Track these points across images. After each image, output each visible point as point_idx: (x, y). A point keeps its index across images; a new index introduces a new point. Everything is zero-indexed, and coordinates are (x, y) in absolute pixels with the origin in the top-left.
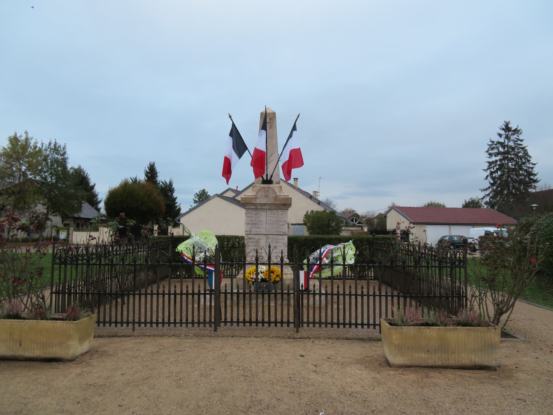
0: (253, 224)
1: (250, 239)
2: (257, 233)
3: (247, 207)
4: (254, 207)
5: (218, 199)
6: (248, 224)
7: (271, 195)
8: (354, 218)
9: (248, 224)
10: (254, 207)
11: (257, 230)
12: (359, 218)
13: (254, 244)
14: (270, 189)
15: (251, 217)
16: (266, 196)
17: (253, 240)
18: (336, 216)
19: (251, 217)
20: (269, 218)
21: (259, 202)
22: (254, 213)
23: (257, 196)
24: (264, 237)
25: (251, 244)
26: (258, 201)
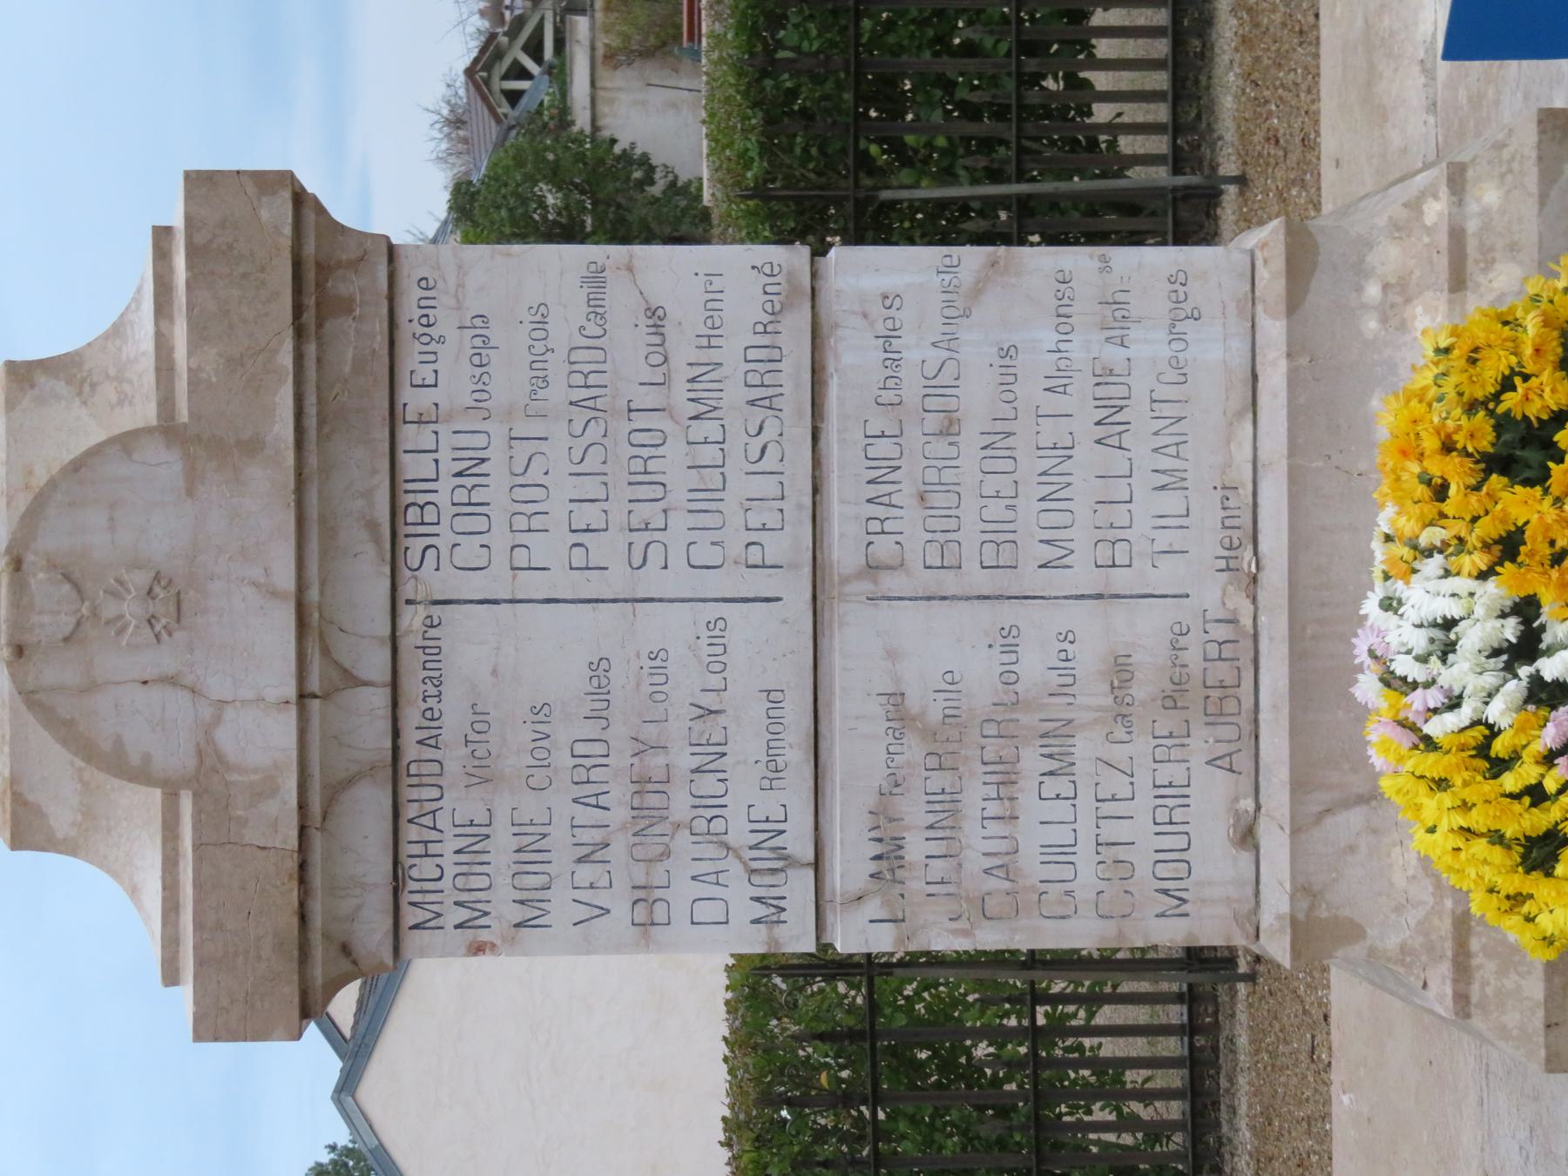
0: (647, 817)
1: (889, 858)
2: (796, 756)
3: (372, 935)
4: (367, 810)
5: (371, 1090)
6: (645, 897)
7: (155, 519)
8: (499, 84)
9: (645, 897)
10: (367, 810)
11: (747, 745)
12: (499, 55)
13: (976, 795)
14: (54, 538)
15: (531, 853)
16: (171, 601)
17: (914, 810)
18: (495, 178)
19: (531, 853)
20: (549, 548)
21: (281, 732)
22: (459, 804)
23: (176, 756)
24: (858, 635)
25: (978, 842)
26: (264, 739)
